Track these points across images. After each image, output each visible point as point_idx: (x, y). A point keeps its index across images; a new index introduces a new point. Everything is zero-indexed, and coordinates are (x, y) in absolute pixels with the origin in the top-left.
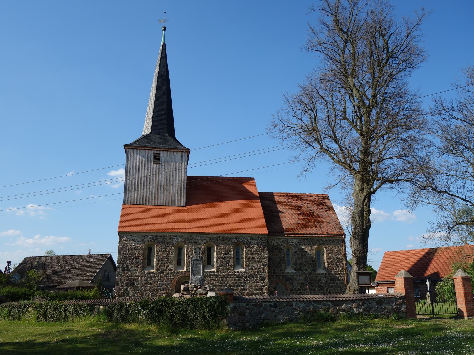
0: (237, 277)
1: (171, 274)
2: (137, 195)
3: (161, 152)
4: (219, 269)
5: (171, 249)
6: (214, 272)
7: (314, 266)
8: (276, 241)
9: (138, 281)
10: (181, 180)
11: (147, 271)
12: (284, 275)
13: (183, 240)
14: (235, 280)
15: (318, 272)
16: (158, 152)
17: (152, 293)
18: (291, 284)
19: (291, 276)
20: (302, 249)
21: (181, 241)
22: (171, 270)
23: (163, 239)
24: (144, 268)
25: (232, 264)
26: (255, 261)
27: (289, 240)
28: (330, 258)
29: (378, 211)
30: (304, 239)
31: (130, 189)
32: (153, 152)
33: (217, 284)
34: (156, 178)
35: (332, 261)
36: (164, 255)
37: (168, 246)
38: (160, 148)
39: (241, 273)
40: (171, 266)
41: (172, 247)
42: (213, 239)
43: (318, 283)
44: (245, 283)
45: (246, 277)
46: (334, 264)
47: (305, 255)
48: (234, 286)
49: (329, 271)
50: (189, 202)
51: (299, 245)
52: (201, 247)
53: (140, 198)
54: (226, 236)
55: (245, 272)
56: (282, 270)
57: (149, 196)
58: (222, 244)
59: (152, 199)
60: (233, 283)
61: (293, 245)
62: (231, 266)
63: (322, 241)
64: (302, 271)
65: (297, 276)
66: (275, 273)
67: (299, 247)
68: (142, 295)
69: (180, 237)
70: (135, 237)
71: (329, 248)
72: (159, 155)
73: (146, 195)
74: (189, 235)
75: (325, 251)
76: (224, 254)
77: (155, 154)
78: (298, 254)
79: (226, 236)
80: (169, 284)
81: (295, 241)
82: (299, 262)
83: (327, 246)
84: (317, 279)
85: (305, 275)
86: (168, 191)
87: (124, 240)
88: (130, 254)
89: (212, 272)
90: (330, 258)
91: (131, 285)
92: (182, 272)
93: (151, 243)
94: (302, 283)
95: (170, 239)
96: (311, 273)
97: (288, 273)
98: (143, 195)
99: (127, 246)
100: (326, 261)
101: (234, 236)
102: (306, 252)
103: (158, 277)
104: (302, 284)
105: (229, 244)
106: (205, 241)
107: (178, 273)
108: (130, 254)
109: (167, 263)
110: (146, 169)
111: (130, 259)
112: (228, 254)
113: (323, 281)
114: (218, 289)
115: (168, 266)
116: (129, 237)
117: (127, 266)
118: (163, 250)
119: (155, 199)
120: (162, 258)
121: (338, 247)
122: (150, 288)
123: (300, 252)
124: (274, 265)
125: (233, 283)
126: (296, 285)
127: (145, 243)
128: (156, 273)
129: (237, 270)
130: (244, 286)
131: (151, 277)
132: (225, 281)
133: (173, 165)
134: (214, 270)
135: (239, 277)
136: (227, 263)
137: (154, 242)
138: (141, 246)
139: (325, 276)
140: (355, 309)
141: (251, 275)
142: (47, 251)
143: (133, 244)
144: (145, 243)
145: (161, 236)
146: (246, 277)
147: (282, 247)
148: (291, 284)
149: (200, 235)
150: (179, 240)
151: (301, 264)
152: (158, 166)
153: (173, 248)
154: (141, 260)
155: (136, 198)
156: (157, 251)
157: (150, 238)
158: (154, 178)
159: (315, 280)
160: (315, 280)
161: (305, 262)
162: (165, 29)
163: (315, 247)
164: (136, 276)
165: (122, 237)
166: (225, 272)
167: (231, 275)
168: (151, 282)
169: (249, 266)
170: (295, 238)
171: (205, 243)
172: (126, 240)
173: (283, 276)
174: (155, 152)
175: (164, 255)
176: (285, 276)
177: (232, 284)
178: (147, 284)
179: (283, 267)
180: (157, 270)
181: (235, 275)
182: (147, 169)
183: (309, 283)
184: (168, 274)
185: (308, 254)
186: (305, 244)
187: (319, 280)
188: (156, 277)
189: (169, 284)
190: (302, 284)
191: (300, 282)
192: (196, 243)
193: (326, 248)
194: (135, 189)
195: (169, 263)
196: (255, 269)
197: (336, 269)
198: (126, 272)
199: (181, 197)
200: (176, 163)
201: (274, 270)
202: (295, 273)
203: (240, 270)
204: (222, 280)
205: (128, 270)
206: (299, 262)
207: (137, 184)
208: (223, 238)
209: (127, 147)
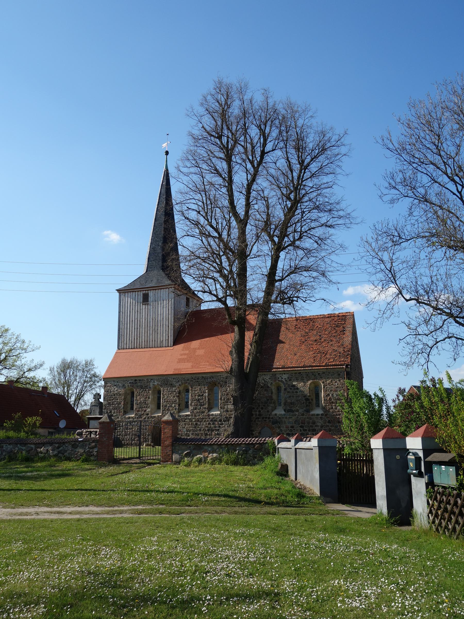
0: (211, 421)
1: (148, 418)
2: (129, 339)
3: (149, 291)
4: (193, 412)
5: (149, 392)
6: (188, 415)
7: (307, 406)
8: (262, 377)
10: (169, 318)
12: (271, 417)
13: (159, 383)
14: (209, 424)
15: (312, 413)
16: (147, 292)
18: (279, 427)
19: (280, 418)
20: (294, 386)
21: (158, 384)
22: (148, 414)
23: (141, 383)
24: (125, 413)
25: (206, 406)
27: (278, 376)
28: (329, 395)
30: (296, 373)
31: (123, 334)
33: (191, 428)
34: (145, 320)
35: (330, 399)
36: (142, 400)
37: (146, 390)
39: (216, 416)
40: (149, 410)
41: (149, 391)
42: (188, 380)
43: (312, 427)
44: (220, 427)
45: (220, 421)
46: (333, 403)
47: (297, 392)
48: (208, 430)
49: (327, 411)
50: (176, 342)
51: (290, 380)
52: (176, 389)
53: (132, 342)
54: (201, 376)
55: (220, 415)
56: (268, 411)
58: (196, 385)
59: (142, 342)
60: (207, 427)
61: (282, 381)
62: (205, 408)
63: (319, 374)
64: (292, 411)
65: (286, 418)
66: (260, 415)
67: (289, 383)
69: (156, 380)
70: (117, 382)
71: (328, 382)
72: (148, 294)
73: (137, 339)
74: (164, 378)
76: (199, 395)
77: (143, 294)
78: (288, 392)
79: (201, 376)
81: (285, 376)
82: (289, 401)
83: (324, 380)
84: (311, 421)
85: (296, 417)
86: (156, 331)
88: (113, 400)
89: (187, 415)
90: (329, 395)
92: (158, 416)
94: (292, 427)
96: (303, 415)
97: (276, 414)
98: (134, 339)
100: (323, 399)
101: (208, 375)
102: (298, 389)
104: (291, 427)
105: (204, 385)
107: (155, 417)
109: (144, 407)
110: (136, 311)
111: (113, 404)
112: (202, 395)
113: (319, 424)
114: (192, 434)
115: (146, 410)
116: (113, 383)
117: (111, 412)
118: (141, 394)
120: (140, 403)
121: (340, 381)
123: (291, 389)
124: (259, 406)
125: (207, 427)
126: (285, 429)
128: (135, 418)
129: (212, 413)
130: (219, 430)
131: (130, 422)
132: (199, 425)
133: (161, 304)
134: (189, 413)
135: (214, 420)
136: (201, 406)
137: (133, 386)
138: (122, 391)
140: (51, 452)
141: (226, 418)
143: (115, 390)
145: (140, 380)
146: (220, 421)
147: (269, 385)
148: (279, 427)
149: (173, 377)
150: (156, 384)
151: (291, 403)
152: (147, 307)
153: (150, 392)
154: (122, 405)
157: (130, 383)
158: (144, 320)
159: (308, 423)
160: (308, 423)
161: (297, 401)
162: (167, 153)
163: (309, 382)
164: (118, 421)
165: (107, 383)
166: (199, 415)
167: (205, 418)
169: (224, 408)
170: (284, 372)
171: (180, 385)
173: (269, 418)
174: (144, 292)
175: (142, 400)
176: (272, 418)
177: (206, 429)
178: (127, 429)
179: (270, 408)
181: (209, 418)
182: (137, 312)
183: (301, 427)
184: (145, 418)
185: (301, 391)
186: (297, 380)
187: (314, 423)
190: (291, 427)
191: (290, 425)
192: (172, 385)
193: (323, 383)
194: (127, 333)
197: (336, 409)
199: (168, 337)
201: (260, 411)
202: (284, 415)
203: (214, 413)
204: (197, 424)
206: (289, 401)
208: (198, 379)
209: (119, 291)
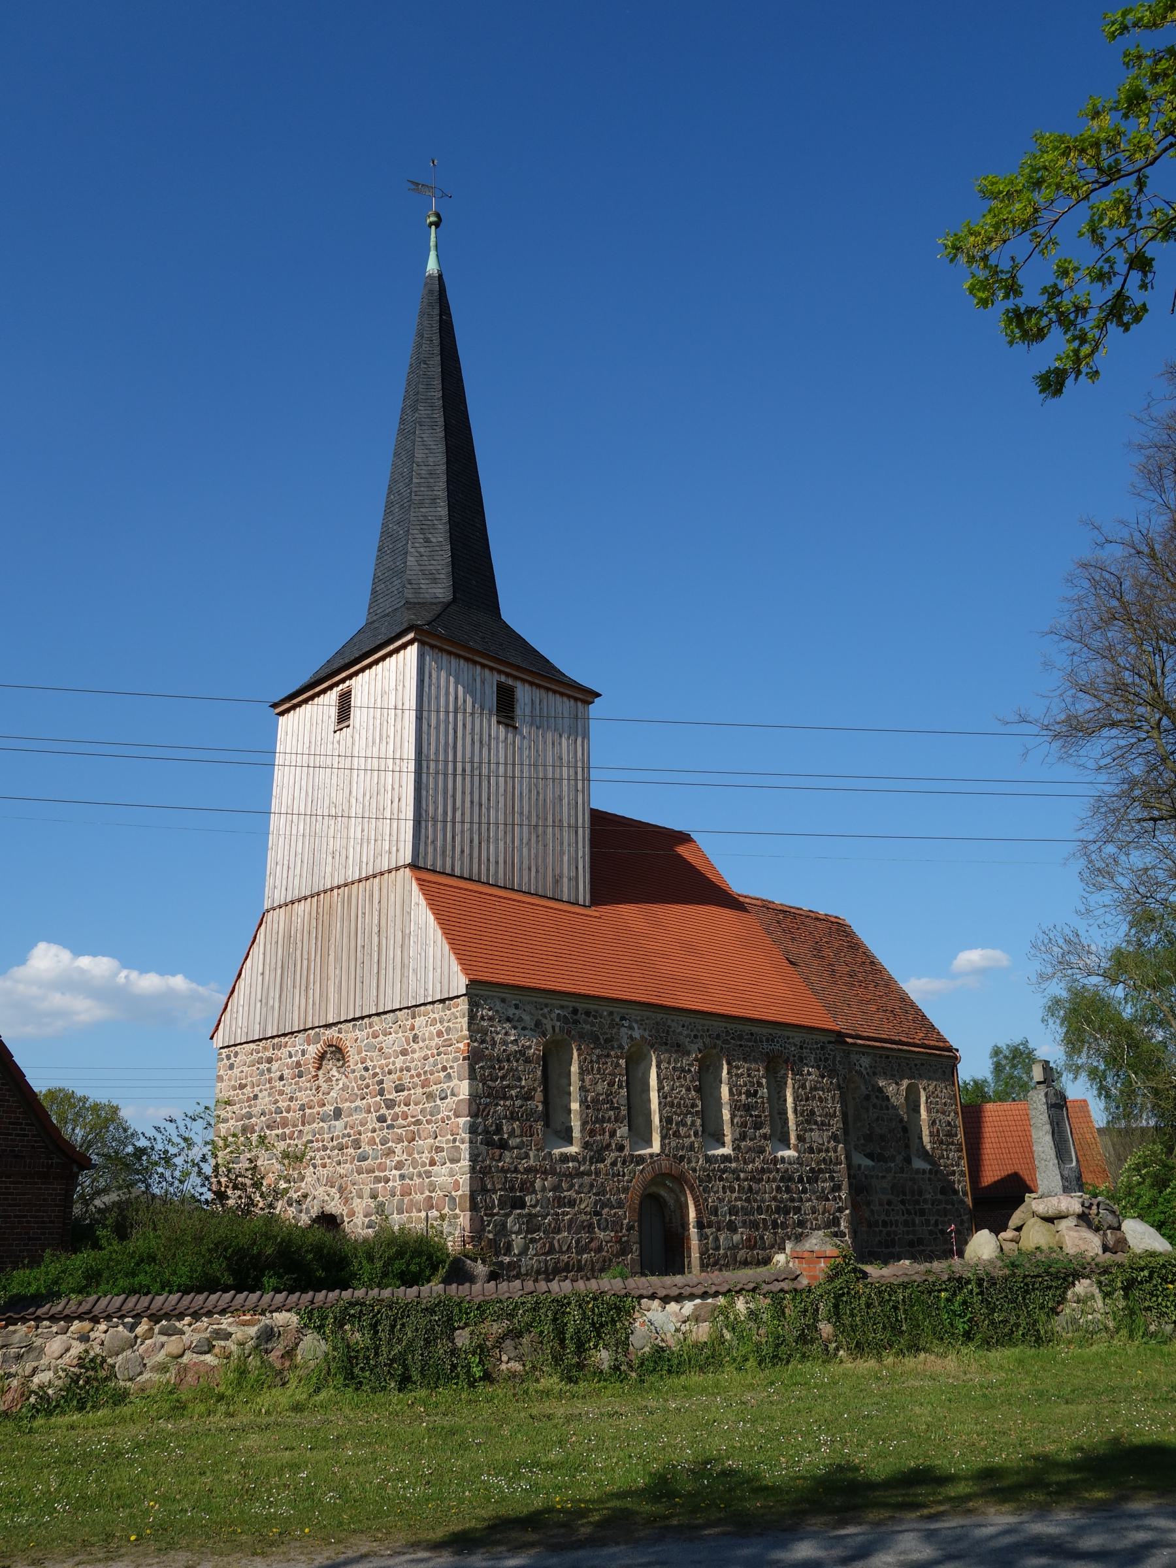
3: (519, 685)
6: (726, 1158)
9: (534, 1192)
11: (556, 1151)
16: (510, 682)
17: (578, 1242)
20: (880, 1090)
26: (816, 1123)
29: (194, 986)
32: (496, 677)
37: (608, 1056)
38: (518, 668)
44: (801, 1200)
47: (888, 1109)
55: (799, 1162)
57: (488, 848)
62: (765, 1137)
68: (551, 1251)
75: (923, 1099)
77: (500, 686)
79: (748, 1028)
80: (620, 1204)
87: (482, 1018)
88: (503, 1078)
91: (514, 1207)
93: (559, 1037)
95: (612, 1026)
99: (494, 1044)
103: (589, 1173)
106: (700, 1045)
108: (503, 1078)
109: (609, 1121)
116: (499, 1006)
117: (499, 1130)
119: (505, 862)
122: (571, 1220)
125: (775, 1199)
127: (545, 1035)
131: (570, 1175)
132: (757, 1193)
139: (930, 1179)
142: (1009, 1042)
144: (545, 1035)
150: (636, 1034)
155: (449, 847)
156: (582, 1072)
163: (905, 1083)
164: (528, 1170)
168: (572, 1193)
172: (491, 1019)
174: (503, 679)
175: (599, 1088)
178: (561, 1202)
180: (586, 1146)
188: (583, 1174)
189: (620, 1204)
193: (924, 1089)
195: (616, 1121)
196: (820, 1151)
198: (497, 1152)
200: (561, 736)
205: (503, 1145)
207: (450, 792)
